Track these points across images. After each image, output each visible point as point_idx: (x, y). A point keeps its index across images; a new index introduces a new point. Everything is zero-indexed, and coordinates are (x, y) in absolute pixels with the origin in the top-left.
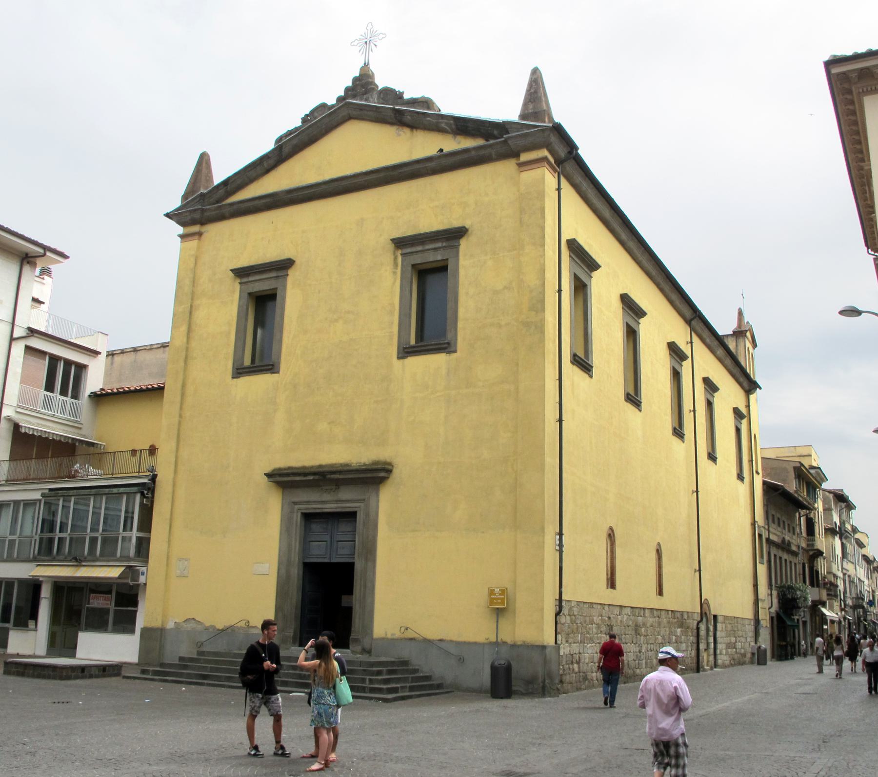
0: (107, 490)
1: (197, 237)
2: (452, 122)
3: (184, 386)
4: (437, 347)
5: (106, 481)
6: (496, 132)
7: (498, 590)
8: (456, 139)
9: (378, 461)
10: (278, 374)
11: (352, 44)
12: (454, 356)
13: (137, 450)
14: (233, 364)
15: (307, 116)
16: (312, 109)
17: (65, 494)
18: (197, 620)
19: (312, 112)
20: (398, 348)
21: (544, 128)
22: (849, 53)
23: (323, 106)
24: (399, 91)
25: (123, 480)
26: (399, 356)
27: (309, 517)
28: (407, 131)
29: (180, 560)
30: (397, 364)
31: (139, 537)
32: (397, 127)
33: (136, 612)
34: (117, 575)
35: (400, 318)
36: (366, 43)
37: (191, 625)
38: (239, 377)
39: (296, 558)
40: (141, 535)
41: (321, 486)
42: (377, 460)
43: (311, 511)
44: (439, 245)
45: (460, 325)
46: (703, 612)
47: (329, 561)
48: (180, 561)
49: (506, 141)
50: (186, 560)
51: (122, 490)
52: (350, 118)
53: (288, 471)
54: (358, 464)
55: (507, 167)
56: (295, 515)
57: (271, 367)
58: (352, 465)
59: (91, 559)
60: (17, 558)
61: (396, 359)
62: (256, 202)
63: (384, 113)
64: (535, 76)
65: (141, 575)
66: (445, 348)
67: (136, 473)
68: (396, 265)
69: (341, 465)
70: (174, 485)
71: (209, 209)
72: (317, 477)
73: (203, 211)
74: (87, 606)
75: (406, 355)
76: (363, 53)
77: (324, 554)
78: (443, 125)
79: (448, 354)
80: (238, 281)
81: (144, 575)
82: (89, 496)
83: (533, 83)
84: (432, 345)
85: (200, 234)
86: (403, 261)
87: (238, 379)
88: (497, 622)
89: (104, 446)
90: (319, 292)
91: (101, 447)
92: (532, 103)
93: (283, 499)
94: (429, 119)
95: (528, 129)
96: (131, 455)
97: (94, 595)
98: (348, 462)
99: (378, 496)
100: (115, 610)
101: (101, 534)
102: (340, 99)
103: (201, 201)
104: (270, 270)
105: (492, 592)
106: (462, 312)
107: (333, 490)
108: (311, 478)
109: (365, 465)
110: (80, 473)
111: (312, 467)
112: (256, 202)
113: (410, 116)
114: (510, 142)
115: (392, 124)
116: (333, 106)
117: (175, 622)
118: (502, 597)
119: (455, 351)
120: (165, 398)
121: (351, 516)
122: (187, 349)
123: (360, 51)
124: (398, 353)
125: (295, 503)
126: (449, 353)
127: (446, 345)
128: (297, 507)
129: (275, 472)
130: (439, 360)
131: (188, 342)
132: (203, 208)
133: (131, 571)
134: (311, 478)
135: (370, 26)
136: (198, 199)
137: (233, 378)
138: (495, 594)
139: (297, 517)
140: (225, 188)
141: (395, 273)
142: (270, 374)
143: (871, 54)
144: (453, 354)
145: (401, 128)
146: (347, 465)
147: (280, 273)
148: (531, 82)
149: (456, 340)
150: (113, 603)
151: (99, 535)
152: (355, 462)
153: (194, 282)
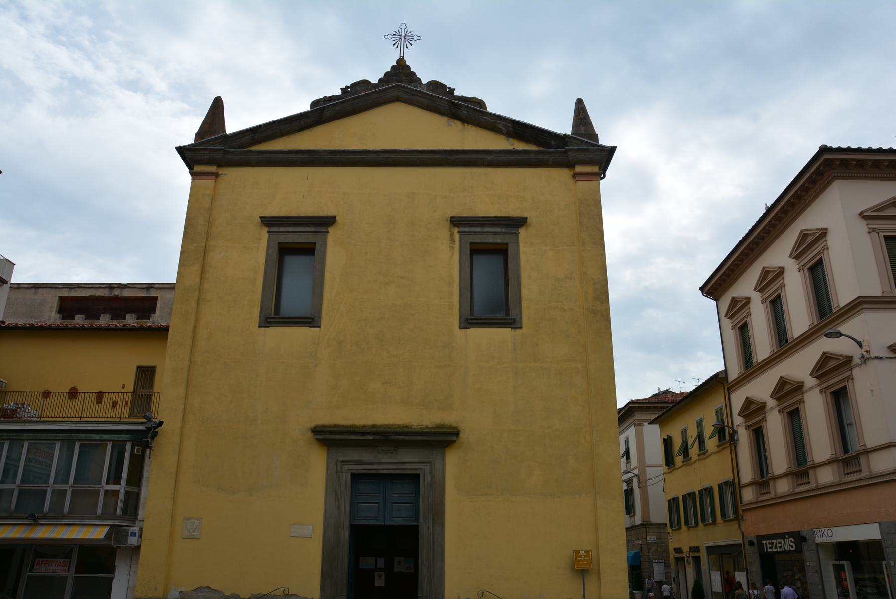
0: (83, 436)
1: (214, 177)
2: (510, 125)
3: (195, 328)
4: (502, 321)
5: (74, 425)
6: (553, 143)
7: (583, 552)
8: (509, 141)
9: (442, 425)
10: (319, 329)
11: (419, 38)
12: (519, 332)
13: (51, 392)
14: (261, 312)
15: (347, 87)
16: (353, 82)
17: (14, 438)
18: (212, 588)
19: (354, 85)
20: (460, 317)
21: (604, 148)
22: (835, 146)
23: (365, 83)
24: (450, 88)
25: (100, 425)
26: (462, 325)
27: (354, 476)
28: (459, 123)
29: (187, 519)
30: (460, 333)
31: (128, 492)
32: (448, 118)
33: (112, 579)
34: (101, 536)
35: (460, 290)
36: (400, 39)
37: (202, 594)
38: (269, 327)
39: (346, 521)
40: (131, 489)
41: (377, 447)
42: (441, 423)
43: (364, 471)
44: (499, 229)
45: (524, 304)
46: (129, 568)
47: (384, 524)
48: (187, 520)
49: (566, 152)
50: (197, 520)
51: (105, 436)
52: (397, 99)
53: (333, 429)
54: (419, 427)
55: (563, 174)
56: (344, 474)
57: (310, 320)
58: (413, 427)
59: (57, 516)
60: (102, 514)
61: (458, 328)
62: (292, 156)
63: (438, 103)
64: (580, 106)
65: (131, 536)
66: (511, 324)
67: (118, 418)
68: (453, 240)
69: (399, 426)
70: (182, 435)
71: (232, 152)
72: (377, 437)
73: (225, 152)
74: (29, 573)
75: (469, 325)
76: (397, 47)
77: (377, 516)
78: (500, 126)
79: (513, 330)
80: (266, 229)
81: (135, 536)
82: (106, 442)
83: (580, 110)
84: (498, 319)
85: (216, 175)
86: (460, 238)
87: (267, 329)
88: (584, 582)
89: (6, 384)
90: (367, 253)
91: (3, 385)
92: (583, 126)
93: (328, 458)
94: (485, 117)
95: (588, 147)
96: (69, 398)
97: (41, 560)
98: (407, 425)
99: (443, 459)
100: (75, 577)
101: (72, 487)
102: (380, 80)
103: (223, 142)
104: (307, 224)
105: (577, 553)
106: (524, 292)
107: (391, 451)
108: (371, 437)
109: (427, 427)
110: (19, 413)
111: (364, 426)
112: (292, 156)
113: (466, 111)
114: (570, 153)
115: (442, 114)
116: (375, 86)
117: (181, 591)
118: (588, 558)
119: (521, 328)
120: (169, 340)
121: (414, 478)
122: (200, 290)
123: (394, 45)
124: (461, 322)
125: (344, 462)
126: (515, 328)
127: (512, 321)
128: (346, 466)
129: (318, 429)
130: (505, 333)
131: (201, 283)
132: (227, 150)
133: (117, 533)
134: (371, 437)
135: (403, 27)
136: (221, 140)
137: (260, 326)
138: (581, 556)
139: (347, 478)
140: (253, 135)
141: (452, 248)
142: (308, 327)
143: (890, 151)
144: (519, 330)
145: (452, 120)
146: (407, 427)
147: (513, 230)
148: (579, 110)
149: (521, 318)
150: (73, 569)
151: (68, 488)
152: (415, 424)
153: (209, 222)
